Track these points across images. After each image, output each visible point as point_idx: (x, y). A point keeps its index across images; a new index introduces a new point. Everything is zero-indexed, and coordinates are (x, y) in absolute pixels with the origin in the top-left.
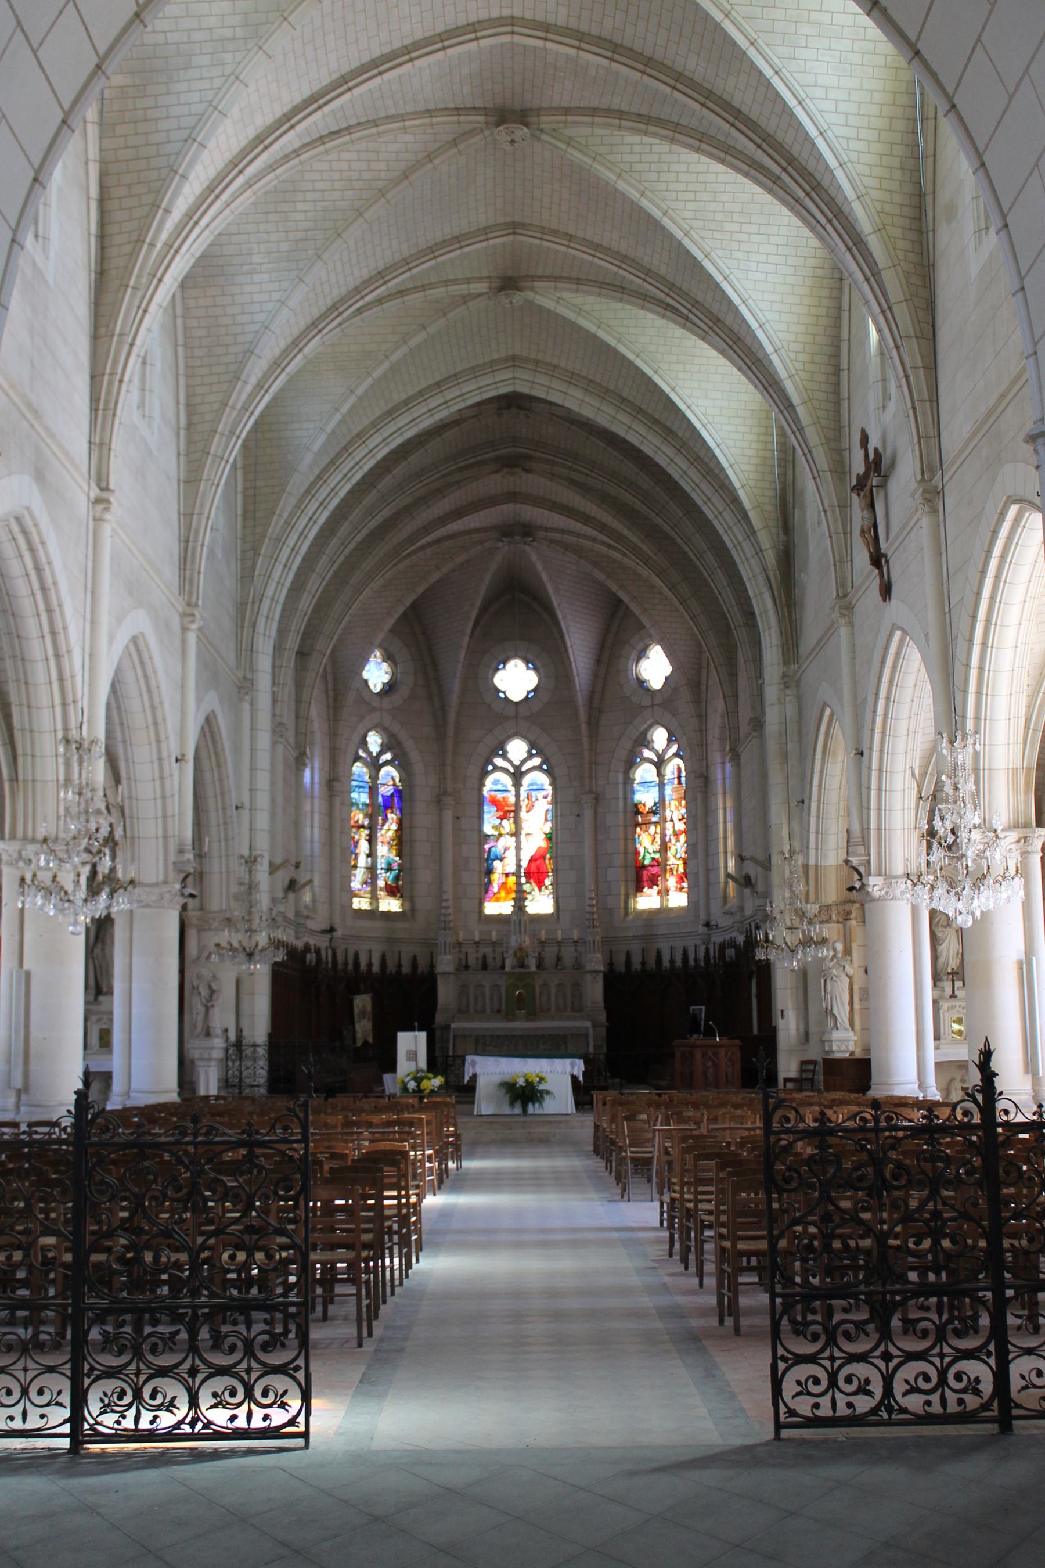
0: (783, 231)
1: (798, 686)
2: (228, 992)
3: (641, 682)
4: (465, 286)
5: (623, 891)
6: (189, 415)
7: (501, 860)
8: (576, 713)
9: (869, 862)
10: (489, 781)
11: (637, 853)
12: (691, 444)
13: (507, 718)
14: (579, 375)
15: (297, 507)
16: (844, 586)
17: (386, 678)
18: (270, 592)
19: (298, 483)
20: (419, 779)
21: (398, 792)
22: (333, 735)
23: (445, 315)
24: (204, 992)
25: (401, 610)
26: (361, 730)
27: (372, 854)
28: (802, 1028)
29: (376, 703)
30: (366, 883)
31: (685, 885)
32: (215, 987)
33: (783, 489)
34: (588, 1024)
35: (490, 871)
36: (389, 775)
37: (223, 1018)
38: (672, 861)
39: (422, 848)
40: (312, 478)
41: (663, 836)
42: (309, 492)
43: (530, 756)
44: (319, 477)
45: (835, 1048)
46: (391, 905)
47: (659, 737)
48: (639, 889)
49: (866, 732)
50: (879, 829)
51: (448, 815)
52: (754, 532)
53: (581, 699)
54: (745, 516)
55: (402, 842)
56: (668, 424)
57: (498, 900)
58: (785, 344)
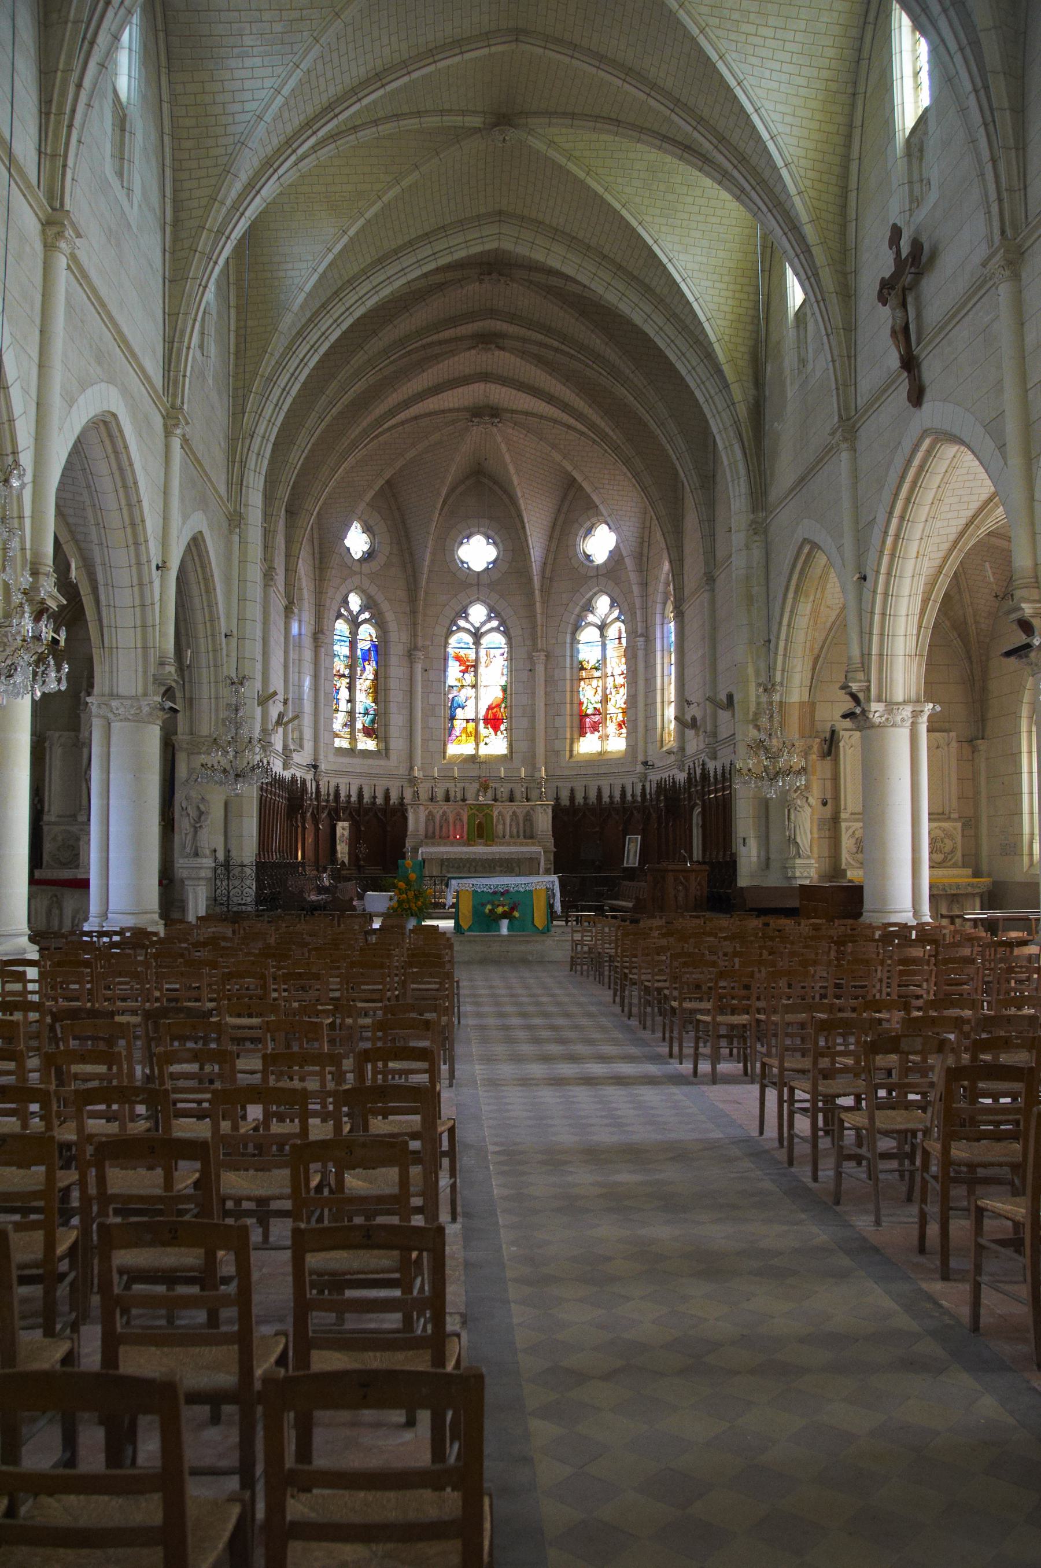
0: (799, 37)
1: (766, 532)
2: (217, 813)
3: (588, 557)
4: (460, 118)
5: (568, 736)
6: (176, 210)
7: (463, 708)
8: (530, 580)
9: (868, 688)
10: (453, 641)
11: (581, 703)
12: (668, 300)
13: (471, 585)
14: (563, 232)
15: (289, 348)
16: (847, 409)
17: (366, 548)
18: (261, 430)
19: (288, 322)
20: (393, 636)
22: (319, 593)
23: (437, 154)
24: (192, 812)
26: (343, 590)
27: (351, 700)
28: (763, 853)
29: (356, 568)
30: (345, 725)
31: (624, 730)
33: (757, 341)
35: (453, 718)
37: (212, 838)
38: (611, 708)
40: (303, 321)
41: (605, 689)
42: (301, 334)
43: (489, 619)
44: (310, 320)
45: (798, 874)
47: (603, 604)
48: (583, 734)
49: (872, 555)
50: (881, 655)
51: (419, 668)
52: (727, 386)
54: (719, 372)
55: (378, 690)
56: (647, 281)
58: (795, 159)
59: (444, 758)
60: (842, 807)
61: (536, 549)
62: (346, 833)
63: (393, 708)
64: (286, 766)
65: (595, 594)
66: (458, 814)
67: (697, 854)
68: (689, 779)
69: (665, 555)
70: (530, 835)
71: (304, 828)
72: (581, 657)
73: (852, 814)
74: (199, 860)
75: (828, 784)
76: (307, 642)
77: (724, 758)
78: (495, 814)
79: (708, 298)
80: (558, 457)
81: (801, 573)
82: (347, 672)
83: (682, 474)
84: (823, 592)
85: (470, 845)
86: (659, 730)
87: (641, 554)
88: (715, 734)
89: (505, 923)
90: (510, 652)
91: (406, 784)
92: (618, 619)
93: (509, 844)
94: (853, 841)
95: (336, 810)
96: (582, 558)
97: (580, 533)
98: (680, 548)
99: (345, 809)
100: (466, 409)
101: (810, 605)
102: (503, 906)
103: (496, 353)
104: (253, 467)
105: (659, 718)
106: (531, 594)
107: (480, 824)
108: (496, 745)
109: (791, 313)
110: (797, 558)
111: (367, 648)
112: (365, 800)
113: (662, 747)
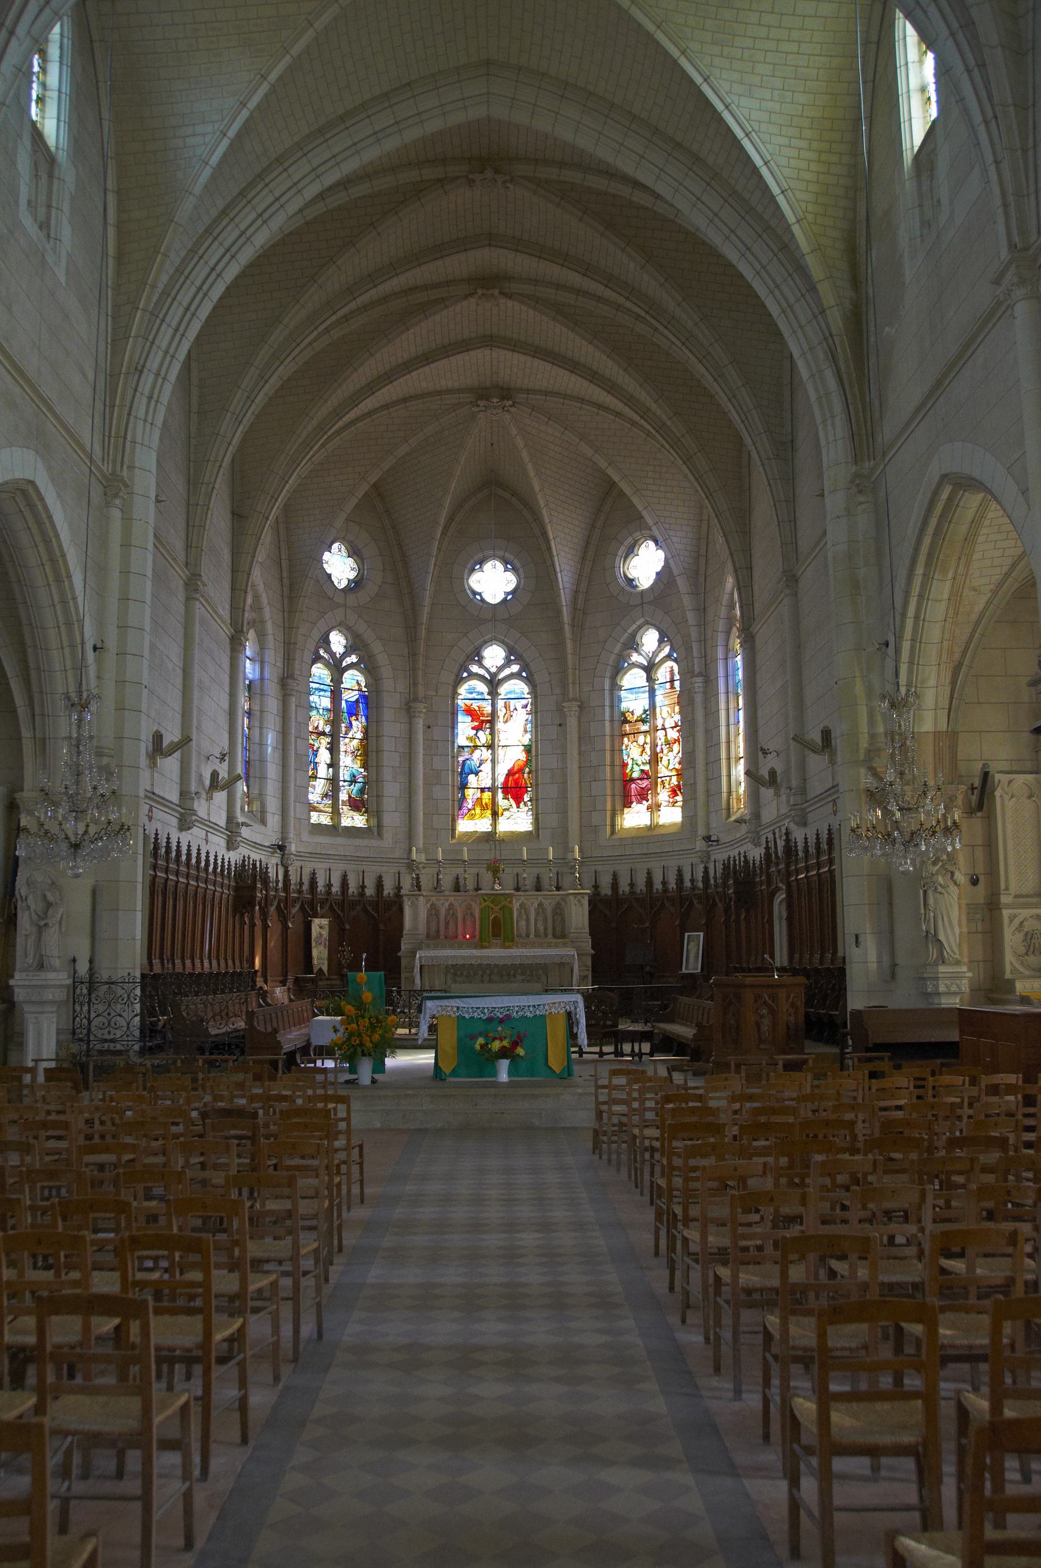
2: (79, 904)
3: (630, 581)
5: (609, 806)
7: (476, 774)
8: (559, 613)
10: (463, 690)
11: (625, 765)
17: (352, 575)
20: (387, 684)
21: (364, 698)
25: (365, 487)
26: (322, 625)
27: (334, 764)
28: (886, 959)
29: (339, 599)
31: (679, 798)
32: (50, 897)
34: (572, 952)
35: (464, 786)
36: (353, 679)
38: (663, 771)
39: (391, 758)
41: (654, 746)
43: (508, 663)
45: (942, 989)
46: (355, 820)
47: (650, 639)
48: (627, 804)
51: (420, 724)
52: (812, 288)
53: (565, 598)
54: (801, 269)
55: (367, 752)
57: (472, 817)
59: (453, 837)
60: (1003, 886)
61: (565, 573)
62: (325, 933)
63: (387, 774)
64: (231, 846)
65: (640, 627)
66: (469, 907)
67: (781, 956)
68: (768, 854)
69: (729, 567)
70: (560, 933)
71: (265, 927)
72: (624, 706)
73: (1016, 896)
74: (43, 975)
75: (979, 853)
76: (272, 689)
77: (819, 822)
78: (516, 905)
79: (783, 162)
80: (589, 452)
81: (936, 533)
82: (328, 729)
83: (748, 440)
84: (968, 565)
85: (482, 947)
86: (724, 795)
87: (697, 573)
88: (803, 790)
89: (504, 1064)
90: (535, 704)
91: (403, 870)
92: (668, 657)
93: (533, 945)
94: (1020, 936)
95: (312, 903)
96: (622, 582)
97: (620, 553)
98: (747, 551)
99: (323, 903)
100: (470, 390)
101: (948, 584)
102: (501, 1039)
103: (502, 301)
104: (141, 414)
105: (724, 779)
106: (558, 631)
107: (496, 919)
108: (517, 820)
109: (908, 158)
110: (929, 510)
111: (353, 699)
112: (350, 891)
113: (729, 816)
